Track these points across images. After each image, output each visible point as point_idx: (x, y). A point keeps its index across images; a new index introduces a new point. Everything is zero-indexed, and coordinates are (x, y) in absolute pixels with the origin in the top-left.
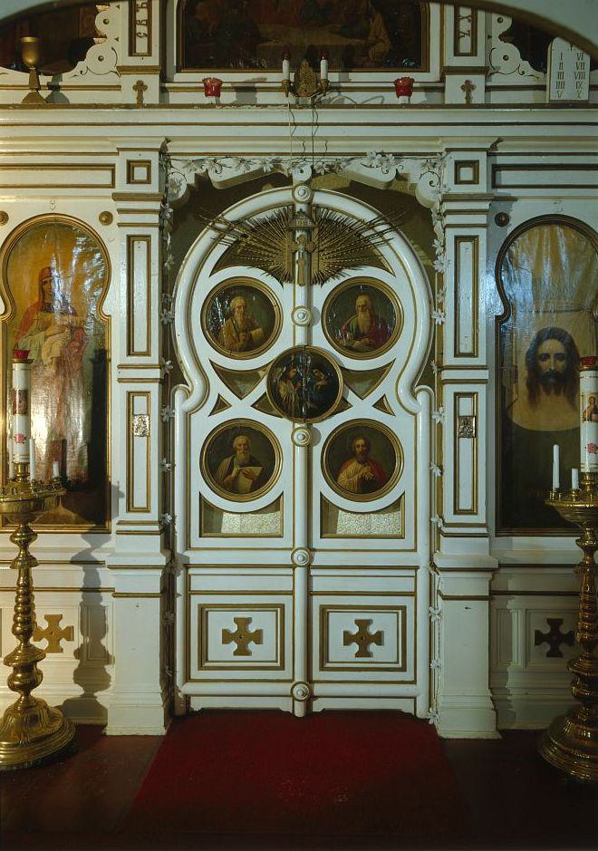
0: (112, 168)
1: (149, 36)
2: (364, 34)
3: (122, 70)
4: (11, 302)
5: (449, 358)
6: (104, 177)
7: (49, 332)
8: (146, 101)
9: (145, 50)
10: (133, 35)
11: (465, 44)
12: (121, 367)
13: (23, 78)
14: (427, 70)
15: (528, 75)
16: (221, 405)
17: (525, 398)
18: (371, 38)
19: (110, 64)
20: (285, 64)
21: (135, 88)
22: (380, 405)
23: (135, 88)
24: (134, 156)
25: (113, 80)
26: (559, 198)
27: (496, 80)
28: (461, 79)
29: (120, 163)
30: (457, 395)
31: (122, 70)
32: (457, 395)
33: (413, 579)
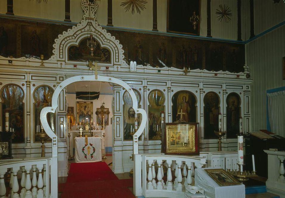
0: (56, 77)
1: (63, 55)
2: (101, 56)
3: (58, 61)
4: (3, 98)
5: (115, 112)
6: (54, 79)
7: (43, 106)
8: (62, 67)
9: (62, 57)
10: (60, 54)
11: (61, 56)
12: (121, 115)
13: (40, 61)
14: (68, 61)
15: (127, 66)
17: (128, 118)
18: (102, 57)
19: (55, 59)
20: (184, 68)
21: (60, 64)
23: (60, 64)
24: (60, 76)
25: (56, 62)
26: (12, 81)
27: (122, 66)
28: (117, 66)
29: (58, 77)
30: (117, 118)
31: (58, 61)
32: (117, 118)
33: (132, 146)
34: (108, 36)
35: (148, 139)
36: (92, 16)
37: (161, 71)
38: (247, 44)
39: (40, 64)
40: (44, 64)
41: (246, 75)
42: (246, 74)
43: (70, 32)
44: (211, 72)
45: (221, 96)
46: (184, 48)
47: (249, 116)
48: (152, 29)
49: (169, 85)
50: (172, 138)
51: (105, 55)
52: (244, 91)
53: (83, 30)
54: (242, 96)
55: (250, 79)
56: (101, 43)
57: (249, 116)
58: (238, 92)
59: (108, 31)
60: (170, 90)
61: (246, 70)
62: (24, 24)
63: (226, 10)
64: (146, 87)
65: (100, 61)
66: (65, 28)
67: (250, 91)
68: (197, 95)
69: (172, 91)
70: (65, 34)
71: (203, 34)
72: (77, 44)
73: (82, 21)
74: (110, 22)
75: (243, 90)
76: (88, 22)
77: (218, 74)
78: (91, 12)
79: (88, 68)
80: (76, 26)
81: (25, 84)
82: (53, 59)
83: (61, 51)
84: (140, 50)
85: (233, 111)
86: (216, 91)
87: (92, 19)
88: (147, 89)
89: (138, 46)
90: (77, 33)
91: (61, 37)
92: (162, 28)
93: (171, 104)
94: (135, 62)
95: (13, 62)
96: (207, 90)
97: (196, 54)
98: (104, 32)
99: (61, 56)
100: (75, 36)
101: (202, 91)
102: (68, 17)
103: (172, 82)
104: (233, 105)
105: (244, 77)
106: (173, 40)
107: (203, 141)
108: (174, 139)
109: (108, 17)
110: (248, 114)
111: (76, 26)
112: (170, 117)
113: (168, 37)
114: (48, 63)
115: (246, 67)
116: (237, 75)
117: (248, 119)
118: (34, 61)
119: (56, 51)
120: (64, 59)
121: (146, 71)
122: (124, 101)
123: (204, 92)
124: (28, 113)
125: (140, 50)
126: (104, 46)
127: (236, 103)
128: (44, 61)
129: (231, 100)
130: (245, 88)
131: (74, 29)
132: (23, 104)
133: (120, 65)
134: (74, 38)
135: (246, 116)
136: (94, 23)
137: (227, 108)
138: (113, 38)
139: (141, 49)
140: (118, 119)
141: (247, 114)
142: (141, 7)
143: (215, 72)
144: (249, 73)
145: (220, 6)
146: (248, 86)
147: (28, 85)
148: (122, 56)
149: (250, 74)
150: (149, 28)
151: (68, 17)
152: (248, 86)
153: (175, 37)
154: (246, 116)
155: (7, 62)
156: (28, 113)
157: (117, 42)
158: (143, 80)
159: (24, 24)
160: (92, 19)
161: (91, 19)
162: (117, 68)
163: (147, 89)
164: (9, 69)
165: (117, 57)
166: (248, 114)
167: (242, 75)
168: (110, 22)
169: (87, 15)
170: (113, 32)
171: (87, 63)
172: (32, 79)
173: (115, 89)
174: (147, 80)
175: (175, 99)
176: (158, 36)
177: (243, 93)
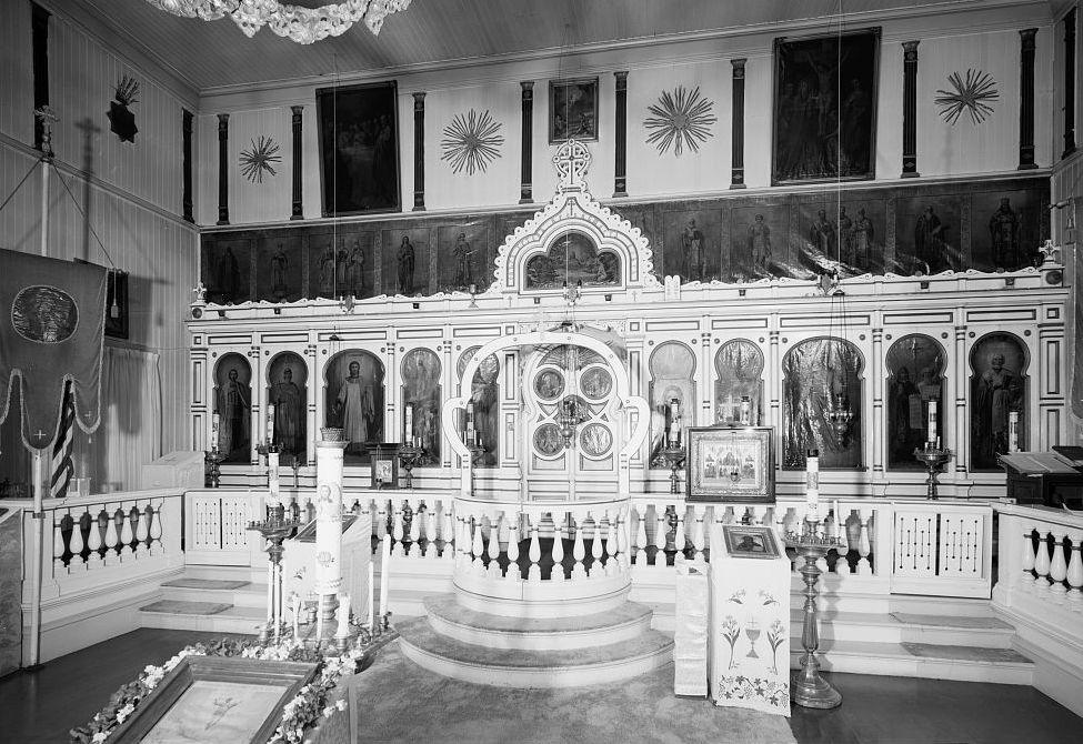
16: (541, 418)
19: (498, 290)
22: (604, 417)
31: (503, 293)
34: (615, 221)
35: (884, 468)
36: (578, 182)
37: (931, 284)
38: (1057, 174)
39: (469, 303)
40: (477, 303)
41: (1048, 275)
42: (1046, 272)
43: (530, 226)
44: (995, 274)
45: (948, 346)
46: (824, 219)
47: (1062, 401)
48: (1018, 165)
49: (774, 324)
50: (708, 460)
51: (607, 268)
52: (1040, 326)
53: (557, 218)
54: (1032, 343)
55: (1062, 287)
56: (538, 249)
57: (1062, 401)
58: (1017, 329)
59: (613, 210)
60: (964, 333)
61: (1049, 258)
62: (442, 224)
63: (975, 86)
64: (881, 330)
65: (595, 280)
66: (522, 218)
67: (1062, 324)
68: (865, 348)
69: (785, 341)
70: (520, 232)
71: (888, 168)
72: (544, 250)
73: (589, 197)
74: (620, 187)
75: (1038, 321)
76: (568, 199)
77: (1017, 280)
78: (575, 174)
79: (822, 291)
80: (543, 211)
81: (700, 339)
82: (494, 289)
83: (511, 271)
84: (695, 244)
85: (996, 388)
86: (934, 332)
87: (578, 190)
88: (967, 335)
89: (691, 235)
90: (544, 228)
91: (510, 240)
92: (313, 212)
93: (322, 383)
94: (677, 278)
95: (421, 305)
96: (899, 332)
97: (864, 232)
98: (604, 214)
99: (511, 283)
100: (540, 233)
101: (964, 333)
102: (526, 196)
103: (886, 313)
104: (998, 371)
105: (1041, 282)
106: (790, 203)
107: (781, 475)
108: (714, 464)
109: (904, 154)
110: (1055, 396)
111: (543, 211)
112: (961, 408)
113: (776, 199)
114: (487, 300)
115: (1049, 249)
116: (275, 309)
117: (1057, 411)
118: (459, 300)
119: (500, 273)
120: (516, 288)
121: (317, 311)
122: (652, 374)
123: (972, 335)
124: (878, 403)
125: (695, 244)
126: (546, 245)
127: (1010, 363)
128: (476, 297)
129: (990, 356)
130: (1042, 317)
131: (539, 218)
132: (439, 388)
133: (641, 287)
134: (536, 238)
135: (1045, 402)
136: (582, 198)
137: (975, 382)
138: (625, 226)
139: (698, 241)
140: (510, 418)
141: (1051, 396)
142: (699, 136)
143: (1007, 274)
144: (1060, 266)
145: (955, 80)
146: (1057, 310)
147: (391, 351)
148: (646, 265)
149: (1062, 269)
150: (281, 216)
151: (526, 196)
152: (1057, 310)
153: (797, 196)
154: (1045, 402)
155: (271, 313)
156: (878, 403)
157: (635, 233)
158: (701, 319)
159: (442, 224)
160: (578, 190)
161: (571, 190)
162: (635, 294)
163: (967, 335)
164: (415, 321)
165: (634, 269)
166: (1055, 396)
167: (1030, 279)
168: (620, 187)
169: (566, 183)
170: (626, 212)
171: (565, 290)
172: (210, 344)
173: (1045, 334)
174: (712, 318)
175: (894, 359)
176: (307, 232)
177: (1035, 332)
